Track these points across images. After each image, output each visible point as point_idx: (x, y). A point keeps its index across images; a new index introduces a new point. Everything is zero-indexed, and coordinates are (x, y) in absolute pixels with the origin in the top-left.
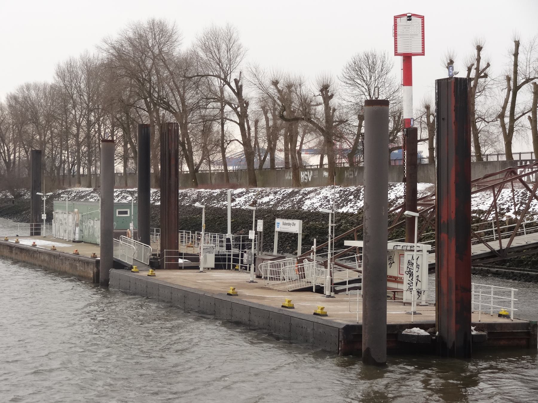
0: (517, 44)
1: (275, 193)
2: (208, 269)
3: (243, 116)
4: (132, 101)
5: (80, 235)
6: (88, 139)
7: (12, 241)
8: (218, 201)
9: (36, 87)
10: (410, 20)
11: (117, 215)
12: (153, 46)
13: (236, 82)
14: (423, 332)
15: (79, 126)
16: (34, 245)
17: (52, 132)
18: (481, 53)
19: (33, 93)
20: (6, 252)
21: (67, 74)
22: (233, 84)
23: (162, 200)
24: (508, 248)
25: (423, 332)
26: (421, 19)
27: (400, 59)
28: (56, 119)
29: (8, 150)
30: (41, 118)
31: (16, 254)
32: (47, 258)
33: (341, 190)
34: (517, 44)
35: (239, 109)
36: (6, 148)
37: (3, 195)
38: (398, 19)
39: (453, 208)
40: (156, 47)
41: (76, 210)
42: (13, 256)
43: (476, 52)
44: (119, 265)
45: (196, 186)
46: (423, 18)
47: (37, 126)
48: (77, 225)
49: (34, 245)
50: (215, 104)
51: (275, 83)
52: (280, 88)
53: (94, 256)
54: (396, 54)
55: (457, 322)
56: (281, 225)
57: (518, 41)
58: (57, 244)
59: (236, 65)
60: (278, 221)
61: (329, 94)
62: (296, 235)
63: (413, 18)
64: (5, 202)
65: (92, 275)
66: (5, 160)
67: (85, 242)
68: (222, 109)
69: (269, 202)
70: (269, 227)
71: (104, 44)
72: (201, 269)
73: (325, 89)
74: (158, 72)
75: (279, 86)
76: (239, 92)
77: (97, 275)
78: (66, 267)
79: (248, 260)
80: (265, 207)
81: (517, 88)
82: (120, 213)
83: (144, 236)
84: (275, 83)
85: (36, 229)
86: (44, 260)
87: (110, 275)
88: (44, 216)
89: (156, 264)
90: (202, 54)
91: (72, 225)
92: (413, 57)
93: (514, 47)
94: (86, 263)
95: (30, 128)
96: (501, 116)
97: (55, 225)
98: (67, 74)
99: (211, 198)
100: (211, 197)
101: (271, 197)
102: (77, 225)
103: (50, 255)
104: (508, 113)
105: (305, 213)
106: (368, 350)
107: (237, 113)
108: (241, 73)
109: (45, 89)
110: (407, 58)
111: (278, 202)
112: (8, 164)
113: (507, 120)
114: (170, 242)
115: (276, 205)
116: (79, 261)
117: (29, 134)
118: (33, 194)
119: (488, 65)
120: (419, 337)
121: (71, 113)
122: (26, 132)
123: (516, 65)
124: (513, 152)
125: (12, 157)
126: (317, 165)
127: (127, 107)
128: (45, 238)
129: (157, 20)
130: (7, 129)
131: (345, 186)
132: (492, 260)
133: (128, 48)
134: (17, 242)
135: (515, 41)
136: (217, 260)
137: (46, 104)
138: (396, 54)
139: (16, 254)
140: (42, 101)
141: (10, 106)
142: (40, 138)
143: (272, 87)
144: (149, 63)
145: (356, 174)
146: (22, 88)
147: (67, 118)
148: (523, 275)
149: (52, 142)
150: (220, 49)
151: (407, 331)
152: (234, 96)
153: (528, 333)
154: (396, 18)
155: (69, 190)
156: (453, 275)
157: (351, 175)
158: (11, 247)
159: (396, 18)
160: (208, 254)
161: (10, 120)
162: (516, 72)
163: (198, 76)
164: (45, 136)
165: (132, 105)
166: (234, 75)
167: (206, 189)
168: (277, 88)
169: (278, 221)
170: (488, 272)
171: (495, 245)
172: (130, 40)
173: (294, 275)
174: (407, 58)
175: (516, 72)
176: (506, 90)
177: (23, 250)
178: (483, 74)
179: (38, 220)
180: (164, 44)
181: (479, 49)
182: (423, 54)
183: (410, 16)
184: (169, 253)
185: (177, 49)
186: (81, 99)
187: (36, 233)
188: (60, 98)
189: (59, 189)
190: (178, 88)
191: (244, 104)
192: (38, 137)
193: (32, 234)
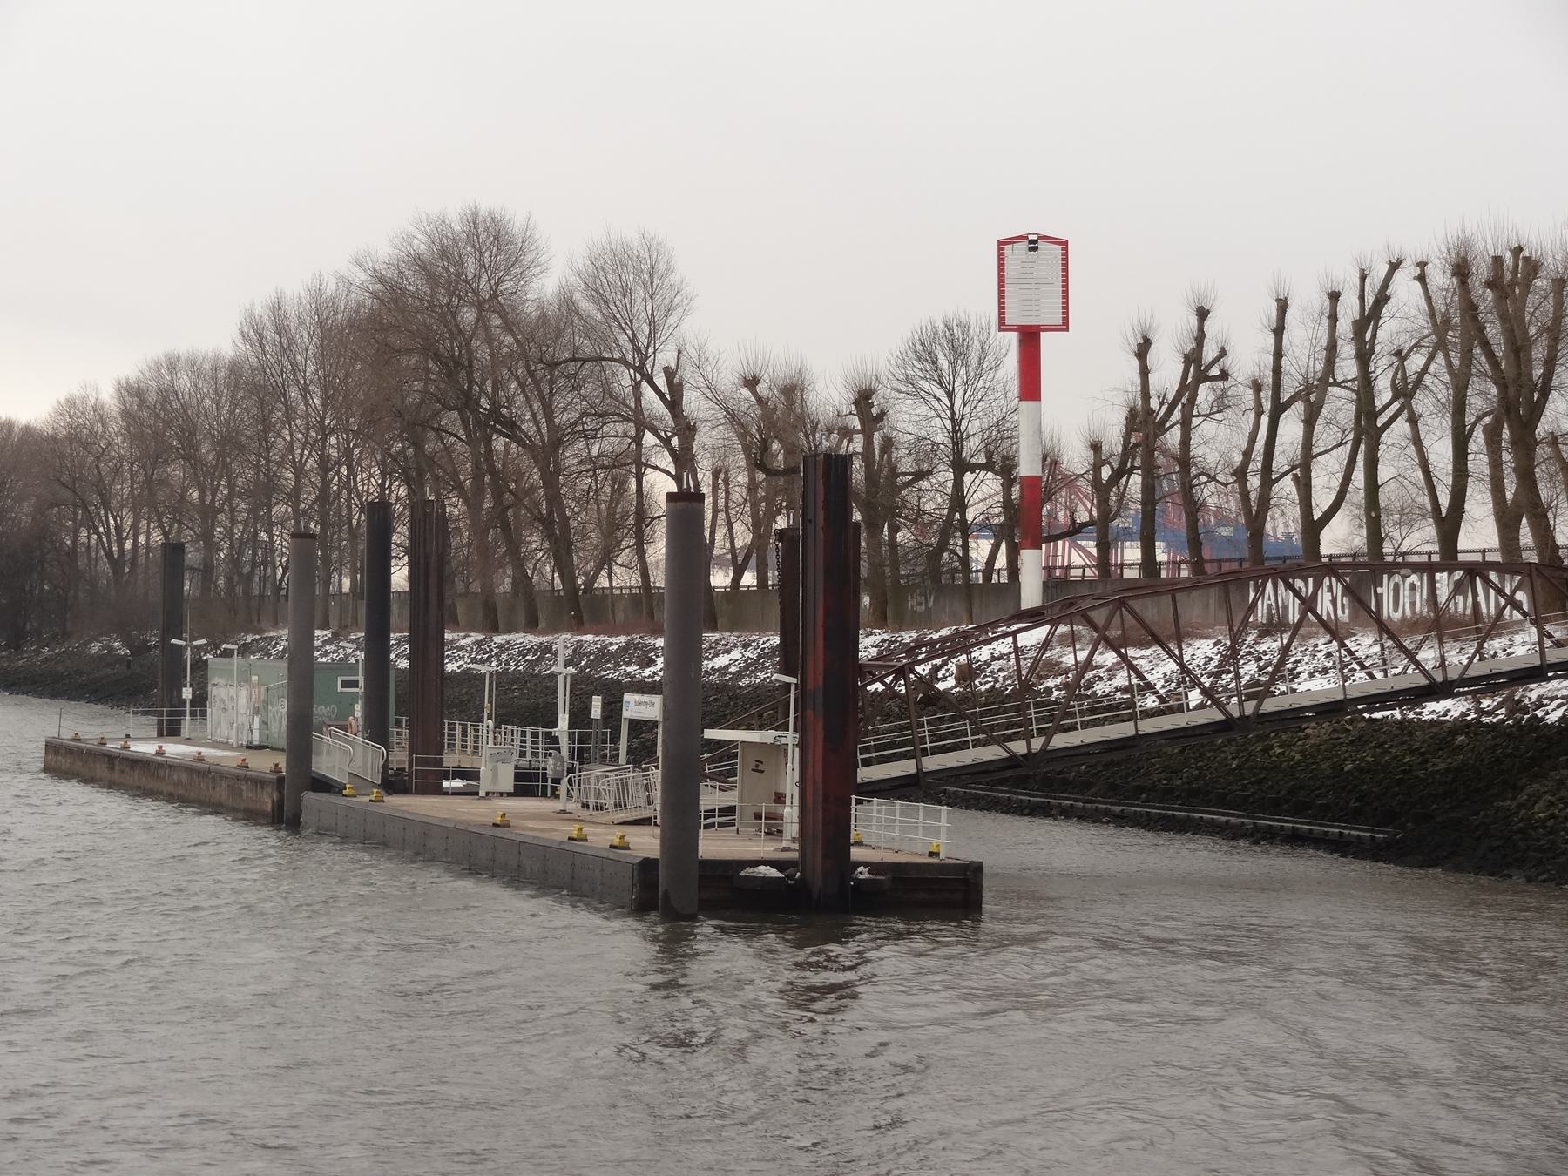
0: (1283, 306)
1: (746, 646)
2: (501, 794)
3: (684, 460)
4: (425, 413)
5: (261, 734)
6: (322, 506)
7: (114, 746)
8: (617, 665)
9: (193, 365)
10: (1036, 249)
11: (339, 689)
12: (477, 277)
13: (669, 374)
14: (774, 873)
15: (299, 472)
16: (160, 753)
17: (231, 486)
18: (1207, 323)
19: (184, 382)
20: (101, 770)
21: (270, 332)
22: (661, 382)
23: (410, 657)
24: (1044, 750)
25: (774, 873)
27: (1014, 337)
28: (242, 449)
29: (119, 528)
30: (205, 448)
31: (122, 771)
32: (184, 777)
33: (884, 641)
34: (1283, 306)
35: (675, 442)
36: (112, 521)
37: (103, 648)
39: (820, 669)
40: (484, 279)
41: (255, 678)
42: (116, 776)
43: (1194, 321)
44: (324, 785)
45: (578, 626)
46: (1064, 244)
47: (194, 468)
48: (256, 711)
49: (160, 753)
50: (620, 428)
51: (751, 383)
53: (277, 769)
54: (1003, 327)
55: (825, 856)
56: (632, 705)
57: (1286, 300)
58: (205, 751)
59: (666, 333)
60: (627, 697)
61: (874, 411)
62: (655, 724)
63: (1041, 244)
64: (108, 665)
65: (269, 807)
66: (109, 554)
67: (272, 749)
68: (638, 440)
69: (727, 667)
70: (613, 709)
71: (357, 269)
72: (482, 794)
73: (863, 399)
74: (490, 340)
75: (762, 389)
76: (674, 404)
77: (279, 806)
78: (222, 794)
79: (554, 770)
80: (716, 679)
81: (1279, 409)
82: (345, 684)
83: (377, 731)
84: (751, 383)
85: (170, 722)
86: (178, 783)
87: (304, 802)
88: (187, 693)
89: (393, 783)
90: (585, 305)
91: (239, 711)
93: (1275, 314)
94: (259, 783)
95: (176, 471)
96: (1241, 473)
97: (212, 711)
98: (271, 334)
99: (604, 655)
100: (604, 655)
101: (735, 655)
102: (256, 711)
103: (190, 770)
104: (1256, 465)
105: (721, 688)
106: (666, 893)
107: (672, 451)
108: (680, 352)
109: (215, 369)
110: (1030, 338)
111: (746, 668)
112: (116, 563)
113: (1254, 482)
114: (428, 743)
115: (739, 675)
116: (247, 779)
117: (172, 486)
118: (164, 640)
119: (1223, 353)
120: (766, 880)
121: (279, 435)
122: (163, 482)
123: (1278, 354)
124: (1460, 547)
125: (128, 545)
127: (416, 427)
128: (188, 741)
129: (483, 211)
130: (117, 471)
131: (894, 631)
132: (1009, 773)
133: (414, 282)
134: (125, 748)
135: (1278, 300)
136: (518, 777)
137: (218, 409)
138: (1003, 327)
139: (122, 771)
140: (207, 402)
141: (126, 414)
142: (202, 497)
143: (746, 392)
144: (468, 316)
145: (931, 604)
146: (157, 366)
147: (268, 450)
148: (1162, 817)
149: (232, 510)
150: (630, 289)
151: (748, 871)
152: (664, 410)
153: (966, 881)
154: (1002, 244)
155: (272, 634)
156: (819, 778)
158: (110, 758)
159: (1002, 244)
160: (500, 765)
161: (121, 447)
162: (1277, 371)
163: (574, 359)
164: (214, 495)
165: (425, 425)
166: (666, 357)
167: (597, 635)
168: (755, 393)
169: (627, 697)
170: (1107, 812)
171: (1019, 747)
172: (419, 263)
173: (643, 802)
174: (1030, 338)
175: (1277, 371)
176: (1252, 415)
177: (137, 763)
178: (1215, 371)
179: (175, 701)
180: (507, 270)
181: (1203, 314)
182: (1065, 327)
183: (1035, 241)
184: (420, 762)
185: (535, 284)
186: (307, 404)
187: (170, 731)
188: (254, 387)
189: (247, 632)
190: (536, 382)
191: (687, 429)
192: (196, 495)
193: (160, 734)
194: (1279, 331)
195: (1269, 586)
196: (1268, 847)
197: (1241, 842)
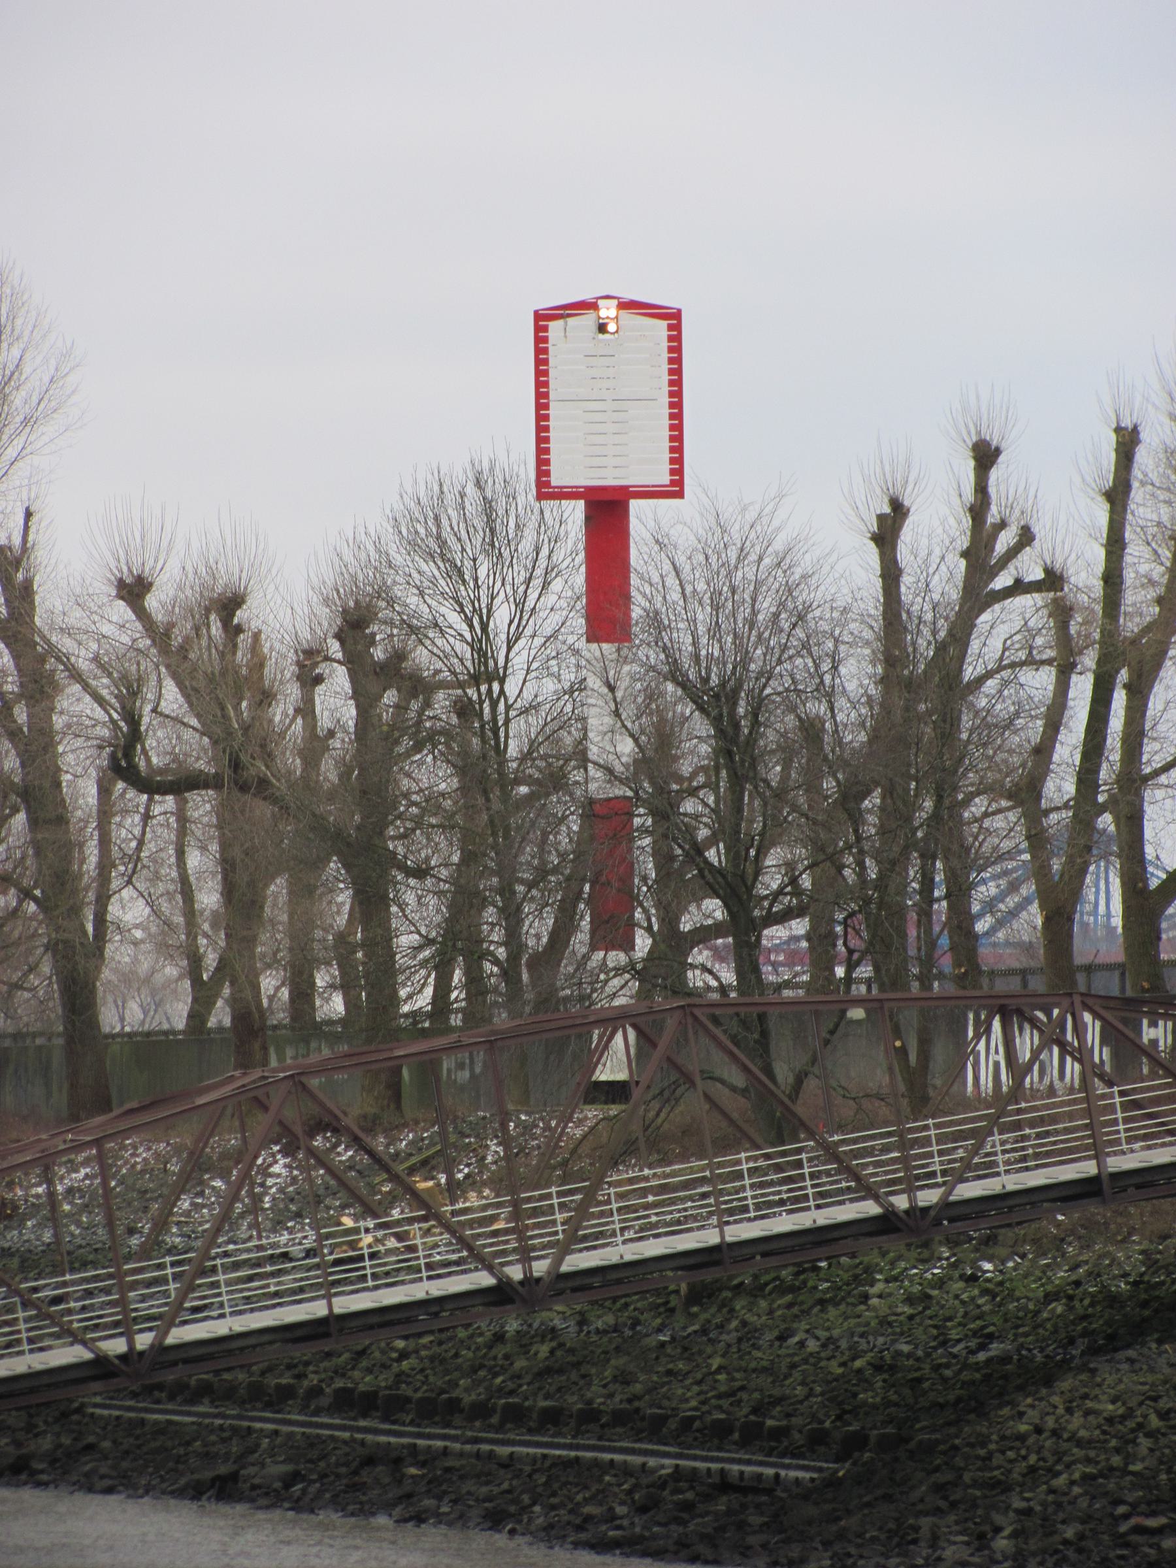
0: (1127, 442)
18: (994, 475)
24: (159, 1349)
26: (663, 324)
27: (576, 511)
34: (1127, 442)
38: (555, 327)
43: (967, 468)
46: (674, 318)
52: (159, 617)
54: (545, 490)
75: (152, 602)
84: (134, 590)
92: (635, 505)
108: (28, 514)
126: (1024, 973)
135: (1118, 430)
143: (122, 611)
154: (542, 319)
157: (461, 1066)
159: (542, 319)
168: (142, 614)
174: (607, 510)
181: (985, 456)
182: (675, 490)
194: (1117, 496)
195: (997, 1024)
196: (335, 1517)
197: (382, 1520)
